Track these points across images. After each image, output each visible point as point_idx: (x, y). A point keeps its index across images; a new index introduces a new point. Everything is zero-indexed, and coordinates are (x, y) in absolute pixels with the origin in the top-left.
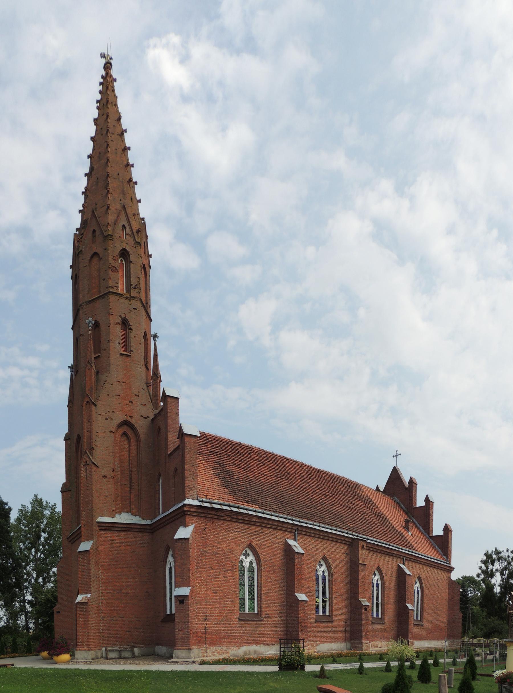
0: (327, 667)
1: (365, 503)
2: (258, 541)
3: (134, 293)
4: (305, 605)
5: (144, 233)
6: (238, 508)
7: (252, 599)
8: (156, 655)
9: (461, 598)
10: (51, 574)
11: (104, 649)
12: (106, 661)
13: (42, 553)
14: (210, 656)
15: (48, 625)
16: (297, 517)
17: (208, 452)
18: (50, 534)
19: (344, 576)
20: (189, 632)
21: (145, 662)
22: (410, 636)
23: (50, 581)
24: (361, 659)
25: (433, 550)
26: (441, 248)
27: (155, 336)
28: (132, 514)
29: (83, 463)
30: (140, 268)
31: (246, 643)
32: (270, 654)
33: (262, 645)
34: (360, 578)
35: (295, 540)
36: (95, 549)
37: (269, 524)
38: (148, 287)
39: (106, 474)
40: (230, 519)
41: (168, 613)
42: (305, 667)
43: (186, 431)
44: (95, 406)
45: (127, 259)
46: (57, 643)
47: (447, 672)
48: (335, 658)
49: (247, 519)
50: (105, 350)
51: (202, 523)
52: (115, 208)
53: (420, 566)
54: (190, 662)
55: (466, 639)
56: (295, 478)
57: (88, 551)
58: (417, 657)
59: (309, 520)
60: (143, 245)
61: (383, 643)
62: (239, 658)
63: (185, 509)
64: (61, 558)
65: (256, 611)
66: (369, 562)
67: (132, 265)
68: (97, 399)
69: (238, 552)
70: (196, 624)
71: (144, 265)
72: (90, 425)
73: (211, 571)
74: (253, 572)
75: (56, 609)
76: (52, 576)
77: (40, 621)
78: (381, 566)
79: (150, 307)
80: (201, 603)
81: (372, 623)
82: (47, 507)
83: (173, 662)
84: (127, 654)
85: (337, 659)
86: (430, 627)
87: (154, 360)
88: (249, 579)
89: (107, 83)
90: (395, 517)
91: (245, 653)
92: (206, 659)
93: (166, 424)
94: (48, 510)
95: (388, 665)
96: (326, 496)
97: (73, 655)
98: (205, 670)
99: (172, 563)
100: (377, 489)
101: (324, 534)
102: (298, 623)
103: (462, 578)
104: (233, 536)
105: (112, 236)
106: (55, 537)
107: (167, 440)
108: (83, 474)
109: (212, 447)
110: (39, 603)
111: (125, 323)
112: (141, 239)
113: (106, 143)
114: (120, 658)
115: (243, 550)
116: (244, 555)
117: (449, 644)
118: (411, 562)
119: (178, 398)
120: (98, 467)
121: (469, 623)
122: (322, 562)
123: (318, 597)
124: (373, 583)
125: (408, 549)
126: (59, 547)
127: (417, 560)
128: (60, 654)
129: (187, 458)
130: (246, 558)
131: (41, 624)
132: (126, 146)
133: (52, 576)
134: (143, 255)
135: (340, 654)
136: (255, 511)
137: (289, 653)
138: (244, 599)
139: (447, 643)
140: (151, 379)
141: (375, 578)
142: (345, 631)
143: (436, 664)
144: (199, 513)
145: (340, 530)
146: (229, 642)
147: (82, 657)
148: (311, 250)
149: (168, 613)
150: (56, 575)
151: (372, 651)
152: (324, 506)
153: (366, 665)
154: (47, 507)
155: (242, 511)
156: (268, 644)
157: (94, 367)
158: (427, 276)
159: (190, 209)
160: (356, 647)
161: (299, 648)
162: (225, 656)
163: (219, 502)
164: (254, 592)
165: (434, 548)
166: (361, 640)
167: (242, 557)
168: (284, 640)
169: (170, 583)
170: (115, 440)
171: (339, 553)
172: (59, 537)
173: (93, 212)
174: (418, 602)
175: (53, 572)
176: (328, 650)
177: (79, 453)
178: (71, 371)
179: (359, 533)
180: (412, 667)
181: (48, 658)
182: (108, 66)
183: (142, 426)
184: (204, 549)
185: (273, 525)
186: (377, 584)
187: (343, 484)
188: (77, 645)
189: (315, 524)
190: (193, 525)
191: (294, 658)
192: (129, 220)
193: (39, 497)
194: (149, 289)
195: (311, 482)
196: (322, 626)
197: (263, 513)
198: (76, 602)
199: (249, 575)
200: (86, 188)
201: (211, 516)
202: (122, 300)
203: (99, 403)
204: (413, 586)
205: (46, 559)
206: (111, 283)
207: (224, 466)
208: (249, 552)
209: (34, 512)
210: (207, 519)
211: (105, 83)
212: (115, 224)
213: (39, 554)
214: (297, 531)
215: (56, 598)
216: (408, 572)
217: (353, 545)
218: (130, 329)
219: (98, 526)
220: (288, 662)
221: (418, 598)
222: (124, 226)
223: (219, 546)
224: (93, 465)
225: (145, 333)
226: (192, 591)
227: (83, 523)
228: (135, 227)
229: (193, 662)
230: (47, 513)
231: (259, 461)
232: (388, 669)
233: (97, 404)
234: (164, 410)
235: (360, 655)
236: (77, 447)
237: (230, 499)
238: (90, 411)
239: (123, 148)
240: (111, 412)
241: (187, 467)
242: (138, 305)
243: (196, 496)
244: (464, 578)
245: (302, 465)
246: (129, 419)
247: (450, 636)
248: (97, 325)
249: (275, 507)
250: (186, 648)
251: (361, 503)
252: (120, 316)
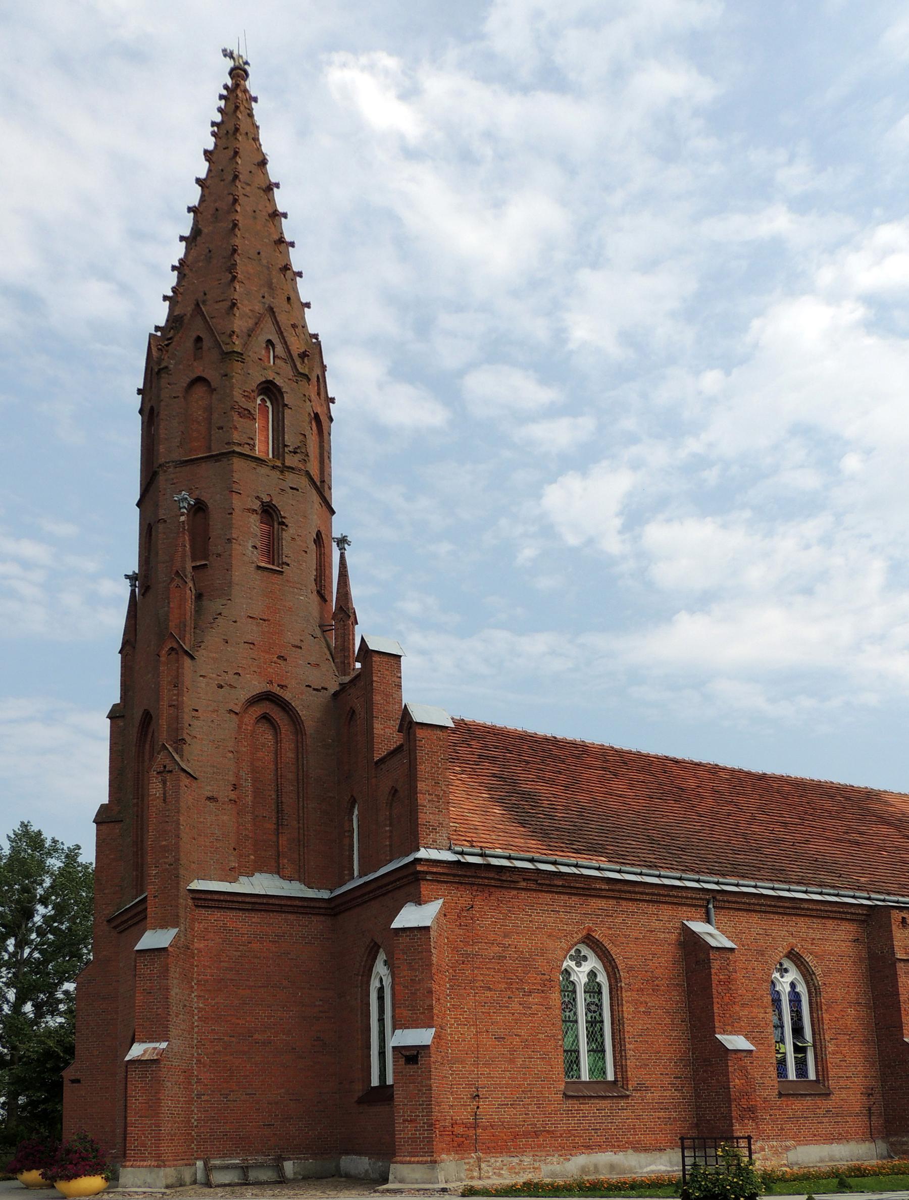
1: (897, 828)
2: (610, 928)
3: (291, 460)
4: (747, 1061)
5: (318, 359)
6: (554, 863)
7: (598, 1051)
8: (341, 1177)
10: (60, 996)
11: (200, 1164)
12: (207, 1190)
13: (36, 949)
15: (45, 1109)
16: (712, 873)
18: (61, 911)
19: (853, 992)
20: (431, 1125)
21: (313, 1192)
23: (54, 1012)
27: (342, 542)
28: (283, 877)
29: (156, 767)
30: (307, 419)
31: (588, 1147)
32: (653, 1172)
33: (630, 1151)
35: (708, 921)
36: (182, 947)
37: (635, 893)
38: (326, 454)
39: (215, 794)
40: (534, 886)
41: (375, 1082)
43: (418, 716)
44: (192, 658)
45: (277, 400)
46: (68, 1152)
49: (578, 885)
50: (219, 555)
51: (463, 897)
52: (250, 308)
54: (434, 1190)
56: (698, 795)
57: (164, 949)
59: (743, 877)
60: (314, 379)
62: (569, 1180)
63: (419, 868)
64: (88, 962)
65: (610, 1077)
67: (287, 411)
68: (198, 645)
69: (559, 952)
70: (450, 1105)
71: (317, 416)
72: (178, 695)
73: (488, 994)
75: (68, 1074)
76: (61, 1001)
77: (22, 1100)
79: (330, 488)
80: (462, 1062)
82: (56, 850)
83: (388, 1191)
84: (265, 1175)
85: (850, 1181)
87: (339, 584)
88: (588, 1010)
89: (236, 102)
91: (584, 1170)
93: (369, 705)
94: (58, 858)
96: (785, 825)
97: (113, 1179)
99: (384, 979)
102: (729, 1101)
104: (536, 924)
105: (242, 354)
106: (75, 917)
108: (155, 789)
110: (20, 1058)
111: (269, 512)
112: (311, 369)
113: (231, 197)
114: (246, 1183)
115: (571, 949)
116: (572, 958)
119: (400, 656)
120: (196, 779)
122: (787, 964)
123: (782, 1041)
126: (86, 938)
128: (76, 1176)
129: (423, 768)
130: (579, 964)
131: (24, 1108)
132: (276, 210)
133: (61, 1001)
134: (314, 396)
136: (599, 869)
137: (711, 1170)
140: (333, 619)
146: (539, 1146)
147: (139, 1183)
148: (711, 380)
149: (375, 1082)
150: (74, 999)
152: (783, 847)
154: (56, 850)
155: (564, 869)
157: (191, 584)
159: (423, 327)
161: (736, 1156)
162: (530, 1176)
167: (569, 963)
169: (381, 1020)
170: (240, 727)
171: (836, 944)
172: (84, 916)
173: (198, 305)
175: (66, 993)
176: (822, 1161)
177: (147, 747)
178: (133, 585)
179: (889, 894)
181: (41, 1187)
182: (239, 73)
183: (309, 706)
184: (469, 950)
185: (647, 894)
187: (832, 797)
188: (125, 1155)
189: (758, 884)
190: (441, 901)
192: (282, 333)
193: (34, 828)
194: (329, 458)
195: (741, 800)
196: (798, 1105)
197: (619, 872)
198: (127, 1058)
199: (589, 1000)
200: (181, 261)
202: (263, 470)
203: (202, 655)
205: (46, 962)
206: (236, 437)
207: (515, 783)
209: (18, 860)
210: (475, 888)
211: (231, 98)
212: (249, 336)
213: (27, 951)
214: (710, 903)
215: (70, 1050)
218: (283, 523)
219: (192, 898)
220: (707, 1189)
222: (270, 342)
223: (507, 942)
224: (183, 775)
225: (319, 534)
226: (437, 1036)
227: (150, 890)
228: (297, 347)
229: (444, 1190)
230: (55, 863)
231: (604, 769)
233: (195, 655)
234: (366, 675)
236: (140, 734)
238: (178, 668)
239: (270, 211)
240: (231, 673)
241: (421, 786)
242: (304, 482)
243: (446, 843)
245: (714, 770)
246: (277, 690)
248: (199, 508)
249: (651, 858)
250: (425, 1159)
251: (884, 830)
252: (258, 498)
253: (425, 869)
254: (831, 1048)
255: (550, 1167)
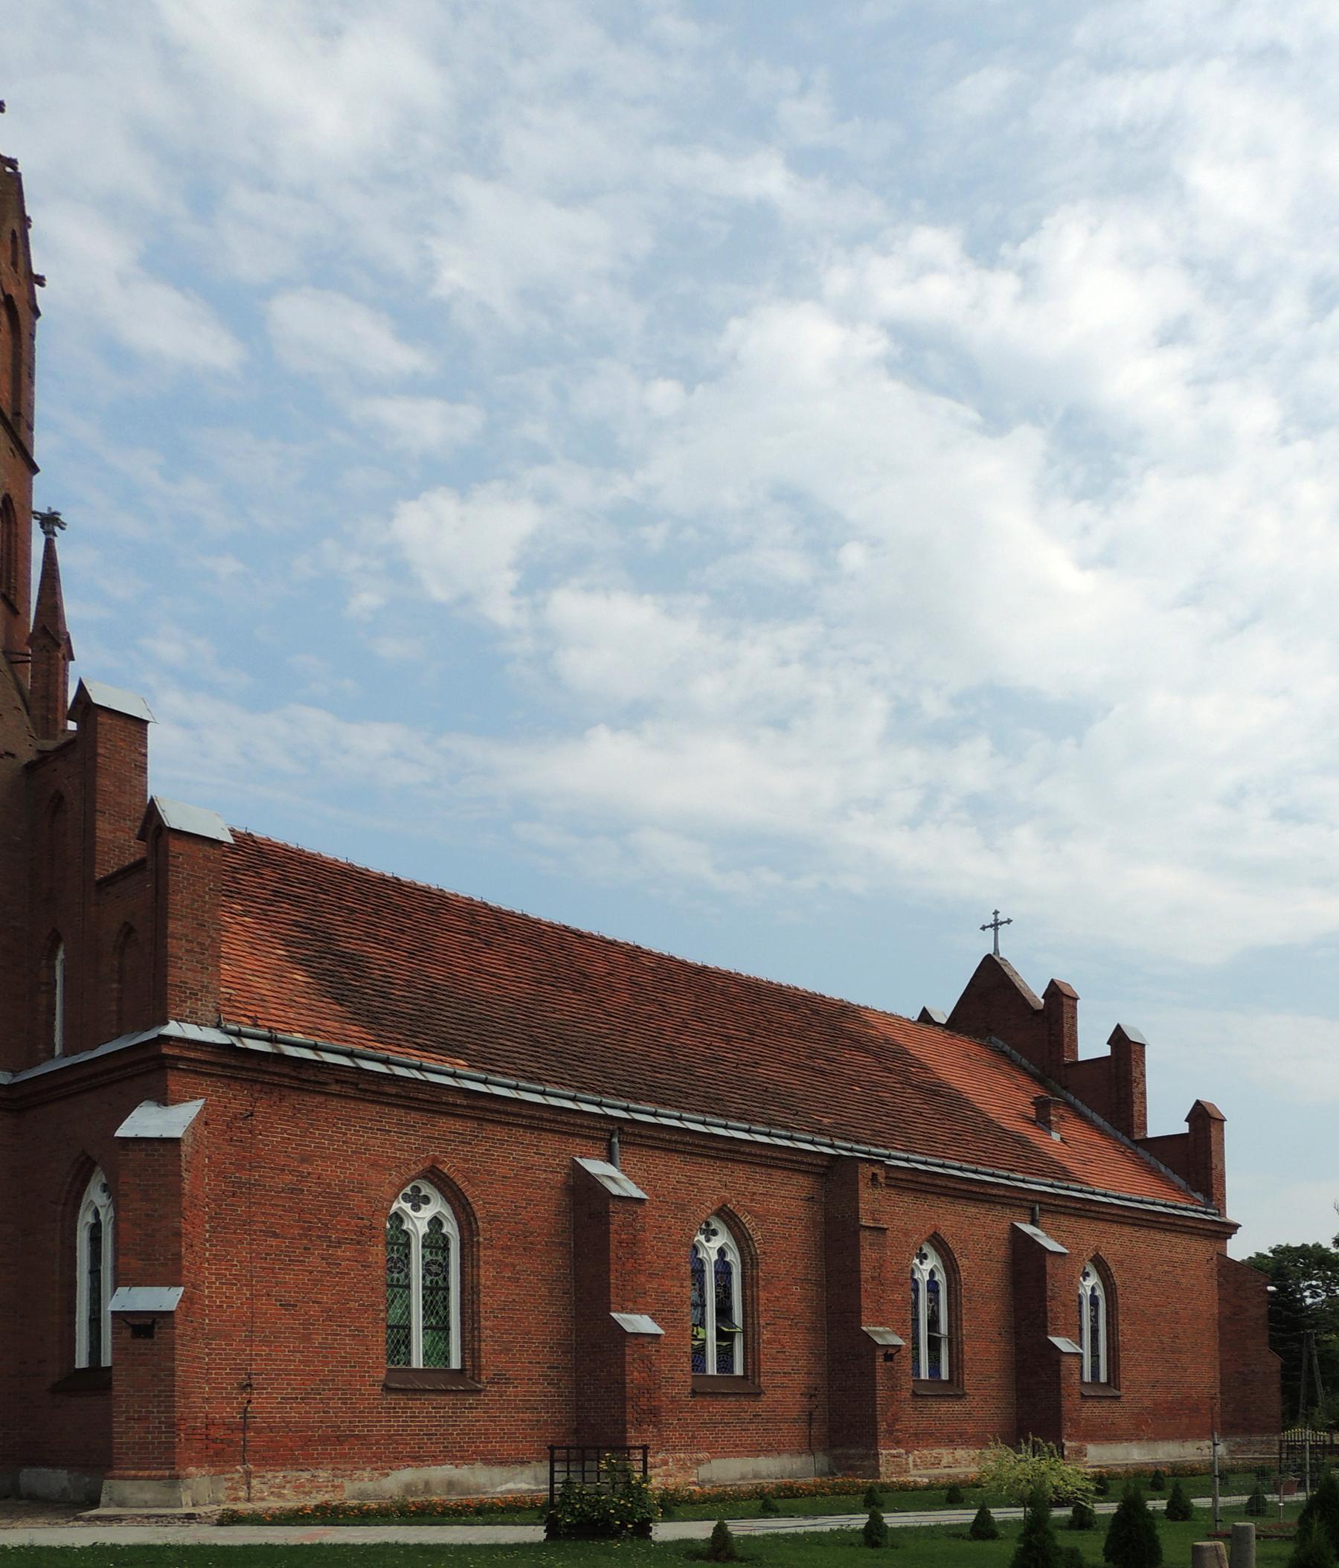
0: (737, 1528)
1: (877, 1057)
2: (466, 1161)
8: (21, 1498)
9: (1270, 1312)
14: (263, 1499)
16: (619, 1095)
17: (266, 894)
22: (1068, 1428)
24: (874, 1500)
25: (1149, 1179)
26: (1140, 384)
27: (51, 521)
31: (415, 1459)
32: (509, 1491)
33: (479, 1465)
34: (866, 1271)
35: (611, 1160)
37: (507, 1114)
40: (352, 1093)
41: (82, 1361)
42: (650, 1529)
43: (176, 816)
47: (1228, 1536)
48: (767, 1501)
51: (238, 1100)
53: (1101, 1226)
54: (174, 1516)
55: (1302, 1434)
58: (1100, 1492)
61: (960, 1453)
62: (385, 1503)
63: (165, 1050)
65: (455, 1363)
66: (897, 1222)
70: (204, 1392)
74: (446, 1248)
78: (943, 1232)
80: (228, 1337)
81: (915, 1395)
83: (99, 1518)
85: (779, 1503)
86: (1147, 1403)
90: (999, 1095)
91: (409, 1489)
92: (242, 1507)
95: (983, 1518)
96: (728, 1039)
98: (239, 1542)
99: (102, 1212)
100: (925, 1017)
101: (721, 1146)
103: (1273, 1251)
107: (94, 836)
109: (284, 880)
116: (406, 1198)
117: (1230, 1452)
118: (1062, 1217)
119: (143, 723)
121: (1311, 1384)
123: (702, 1324)
124: (915, 1282)
125: (1049, 1181)
127: (1087, 1210)
129: (178, 901)
130: (416, 1208)
135: (790, 1488)
136: (453, 1075)
137: (589, 1488)
138: (408, 1328)
139: (1221, 1449)
141: (922, 1273)
142: (811, 1420)
143: (1179, 1511)
144: (224, 1066)
145: (784, 1133)
146: (343, 1456)
148: (665, 394)
149: (82, 1361)
151: (919, 1476)
153: (893, 1520)
156: (502, 1463)
158: (1089, 451)
159: (204, 201)
160: (851, 1468)
161: (627, 1473)
162: (327, 1497)
163: (311, 1040)
164: (446, 1308)
165: (1153, 1171)
166: (873, 1443)
167: (401, 1205)
168: (568, 1448)
171: (783, 1204)
174: (1095, 1332)
176: (743, 1478)
179: (857, 1142)
180: (1082, 1520)
185: (524, 1117)
186: (933, 1286)
189: (684, 1115)
190: (201, 1102)
191: (606, 1501)
195: (669, 999)
196: (717, 1408)
199: (429, 1257)
201: (276, 1079)
204: (1073, 1286)
208: (426, 1189)
210: (258, 1087)
214: (611, 1137)
216: (1052, 1245)
217: (834, 1177)
221: (1095, 1319)
223: (306, 1168)
229: (190, 1517)
231: (470, 934)
232: (983, 1529)
235: (870, 1491)
237: (357, 1037)
243: (212, 1016)
244: (1283, 1253)
247: (1234, 1421)
249: (533, 1067)
250: (160, 1473)
251: (861, 1058)
253: (176, 1052)
254: (766, 1335)
255: (358, 1485)
